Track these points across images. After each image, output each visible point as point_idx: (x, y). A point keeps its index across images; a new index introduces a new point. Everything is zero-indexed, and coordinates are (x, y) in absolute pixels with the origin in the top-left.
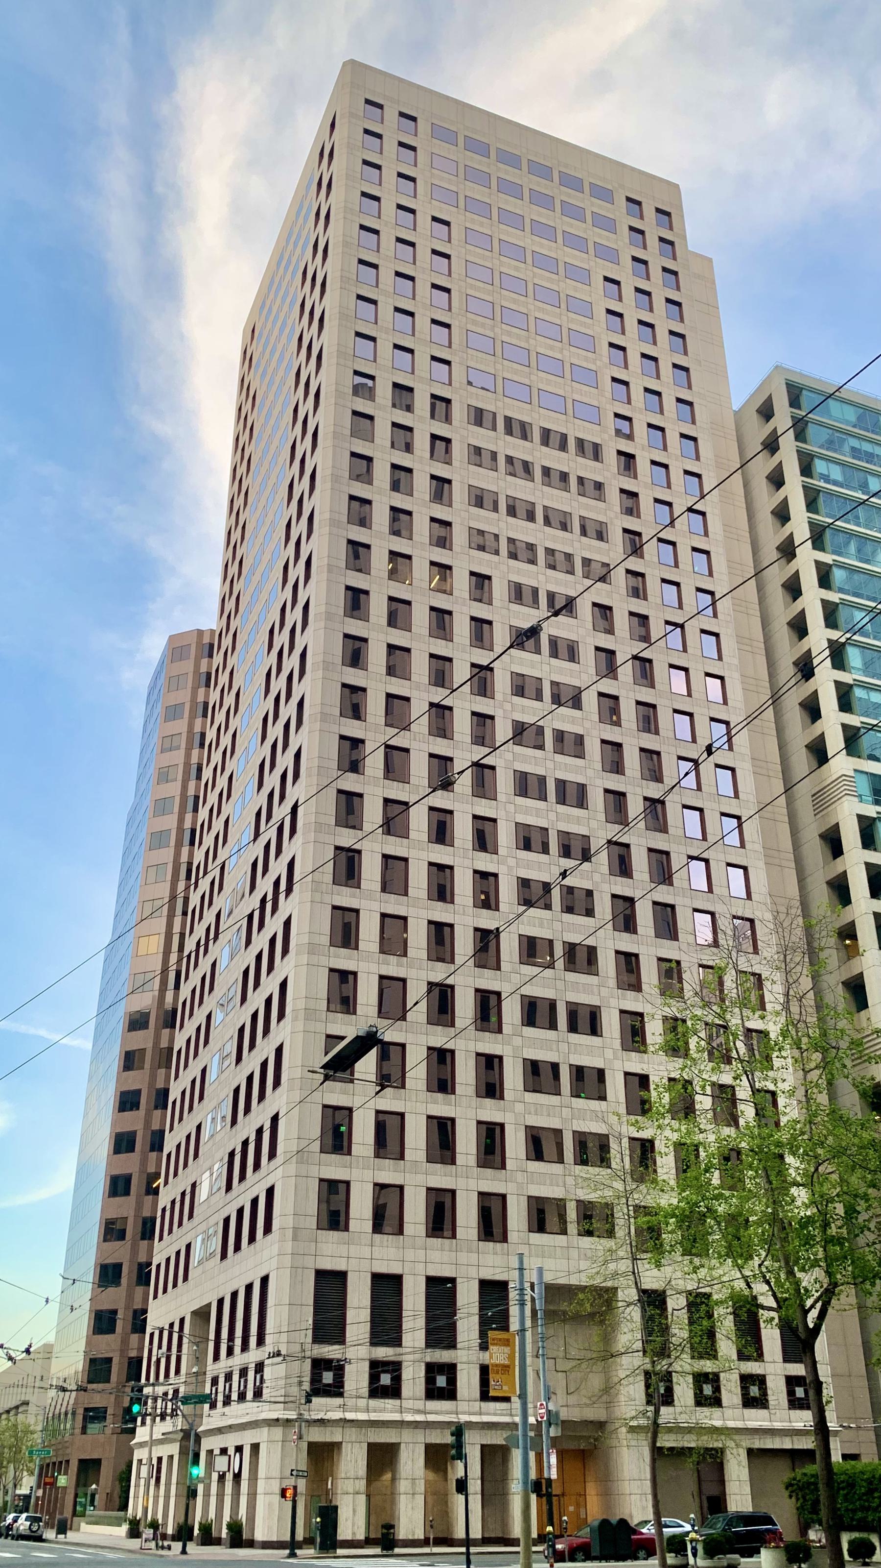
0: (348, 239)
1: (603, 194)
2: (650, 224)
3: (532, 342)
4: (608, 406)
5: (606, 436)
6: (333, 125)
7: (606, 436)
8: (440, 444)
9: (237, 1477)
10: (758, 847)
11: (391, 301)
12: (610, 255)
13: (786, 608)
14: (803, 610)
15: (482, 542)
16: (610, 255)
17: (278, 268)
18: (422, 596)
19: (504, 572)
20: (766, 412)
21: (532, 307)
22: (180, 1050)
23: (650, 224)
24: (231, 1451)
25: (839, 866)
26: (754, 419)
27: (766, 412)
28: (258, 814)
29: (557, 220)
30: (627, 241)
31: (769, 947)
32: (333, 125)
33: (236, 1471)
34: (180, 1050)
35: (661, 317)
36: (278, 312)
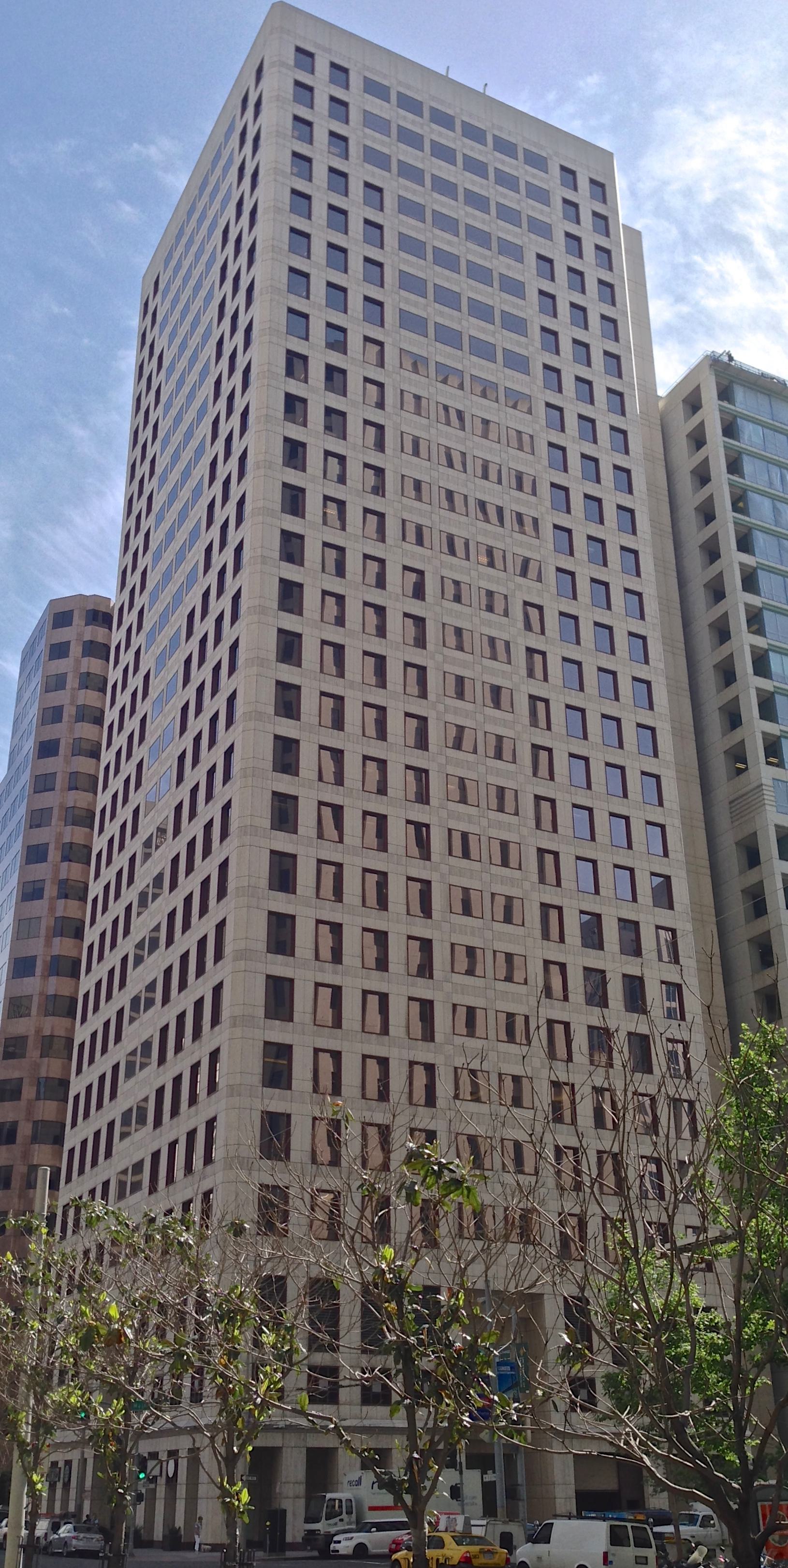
0: (280, 205)
1: (537, 161)
2: (583, 196)
3: (464, 323)
4: (539, 396)
5: (537, 427)
6: (260, 71)
7: (537, 427)
8: (339, 105)
9: (172, 1482)
10: (681, 857)
11: (323, 275)
12: (543, 230)
13: (724, 735)
14: (712, 495)
15: (372, 156)
16: (543, 230)
17: (201, 194)
18: (356, 640)
19: (394, 187)
20: (693, 403)
21: (465, 286)
22: (97, 897)
23: (583, 196)
24: (163, 1456)
25: (737, 735)
26: (680, 411)
27: (693, 403)
28: (182, 758)
29: (491, 190)
30: (561, 215)
31: (688, 959)
32: (260, 71)
33: (171, 1475)
34: (97, 897)
35: (594, 336)
36: (199, 228)
